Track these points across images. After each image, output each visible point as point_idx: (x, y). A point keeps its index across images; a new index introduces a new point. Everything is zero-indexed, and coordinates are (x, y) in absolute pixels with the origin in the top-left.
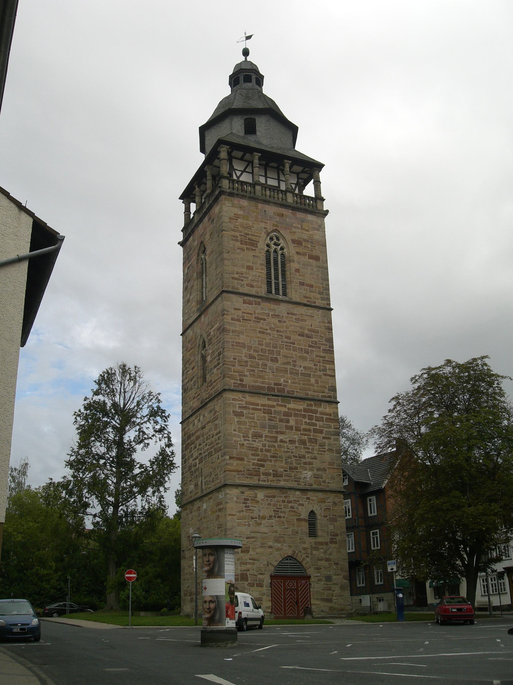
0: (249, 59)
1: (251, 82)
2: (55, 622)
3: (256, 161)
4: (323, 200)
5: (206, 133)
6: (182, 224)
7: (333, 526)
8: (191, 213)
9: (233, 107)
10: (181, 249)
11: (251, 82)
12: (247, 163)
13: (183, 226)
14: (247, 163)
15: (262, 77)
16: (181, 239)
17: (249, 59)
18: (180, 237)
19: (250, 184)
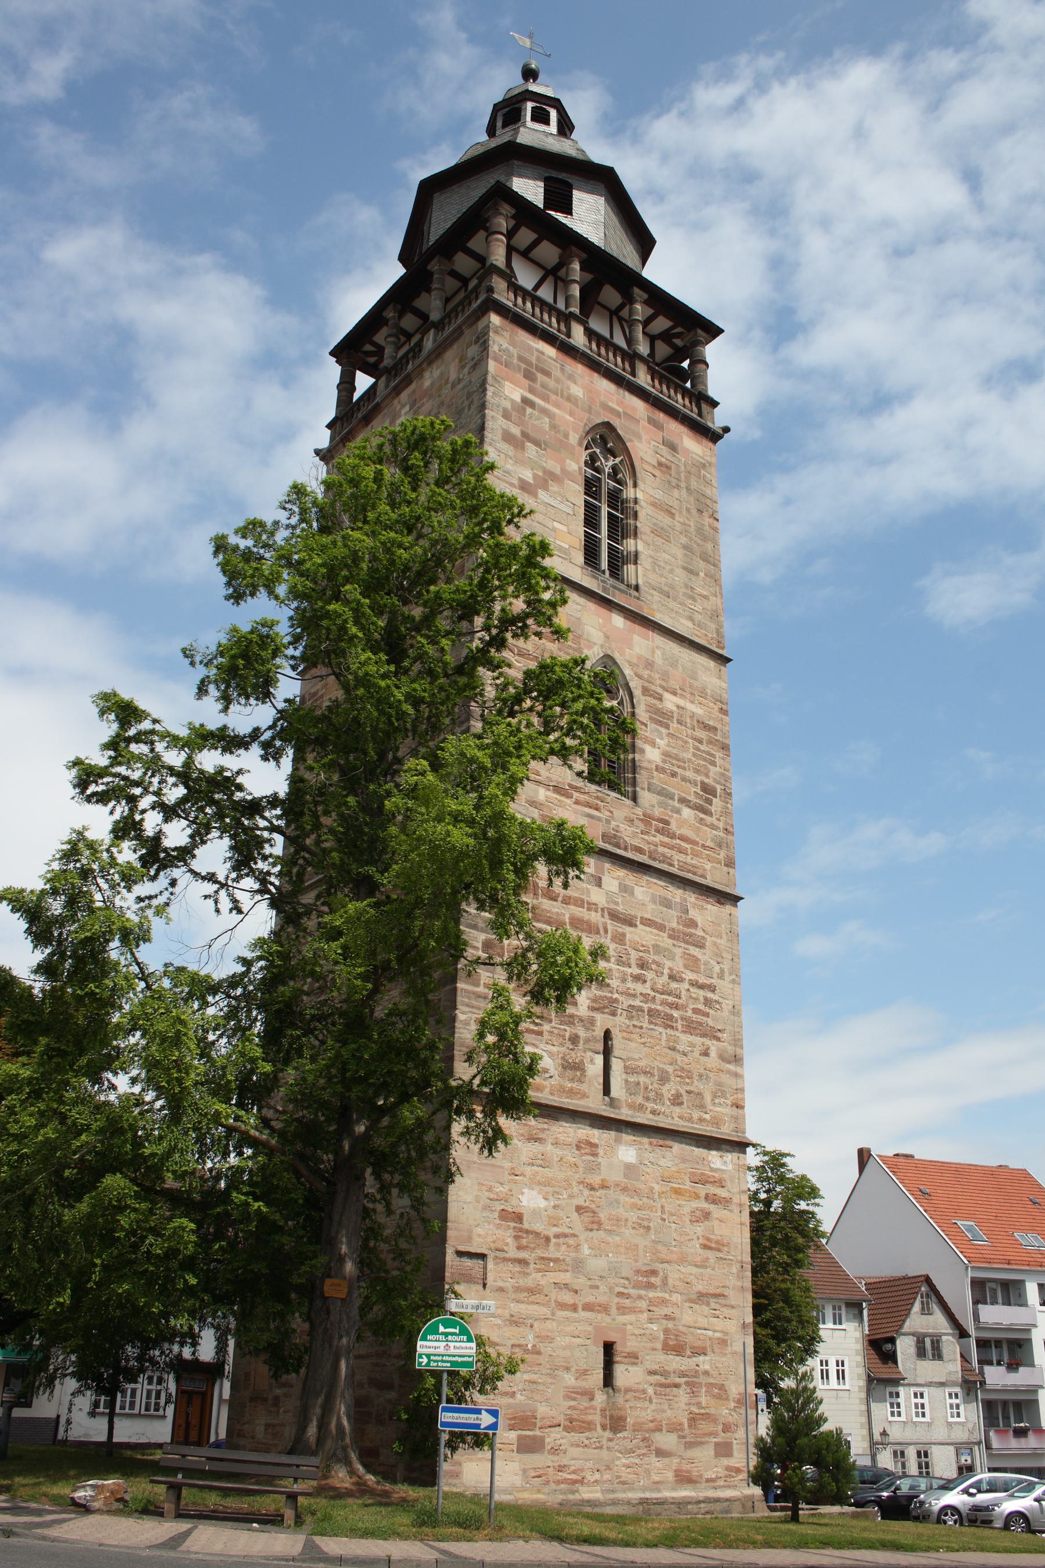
6: (330, 413)
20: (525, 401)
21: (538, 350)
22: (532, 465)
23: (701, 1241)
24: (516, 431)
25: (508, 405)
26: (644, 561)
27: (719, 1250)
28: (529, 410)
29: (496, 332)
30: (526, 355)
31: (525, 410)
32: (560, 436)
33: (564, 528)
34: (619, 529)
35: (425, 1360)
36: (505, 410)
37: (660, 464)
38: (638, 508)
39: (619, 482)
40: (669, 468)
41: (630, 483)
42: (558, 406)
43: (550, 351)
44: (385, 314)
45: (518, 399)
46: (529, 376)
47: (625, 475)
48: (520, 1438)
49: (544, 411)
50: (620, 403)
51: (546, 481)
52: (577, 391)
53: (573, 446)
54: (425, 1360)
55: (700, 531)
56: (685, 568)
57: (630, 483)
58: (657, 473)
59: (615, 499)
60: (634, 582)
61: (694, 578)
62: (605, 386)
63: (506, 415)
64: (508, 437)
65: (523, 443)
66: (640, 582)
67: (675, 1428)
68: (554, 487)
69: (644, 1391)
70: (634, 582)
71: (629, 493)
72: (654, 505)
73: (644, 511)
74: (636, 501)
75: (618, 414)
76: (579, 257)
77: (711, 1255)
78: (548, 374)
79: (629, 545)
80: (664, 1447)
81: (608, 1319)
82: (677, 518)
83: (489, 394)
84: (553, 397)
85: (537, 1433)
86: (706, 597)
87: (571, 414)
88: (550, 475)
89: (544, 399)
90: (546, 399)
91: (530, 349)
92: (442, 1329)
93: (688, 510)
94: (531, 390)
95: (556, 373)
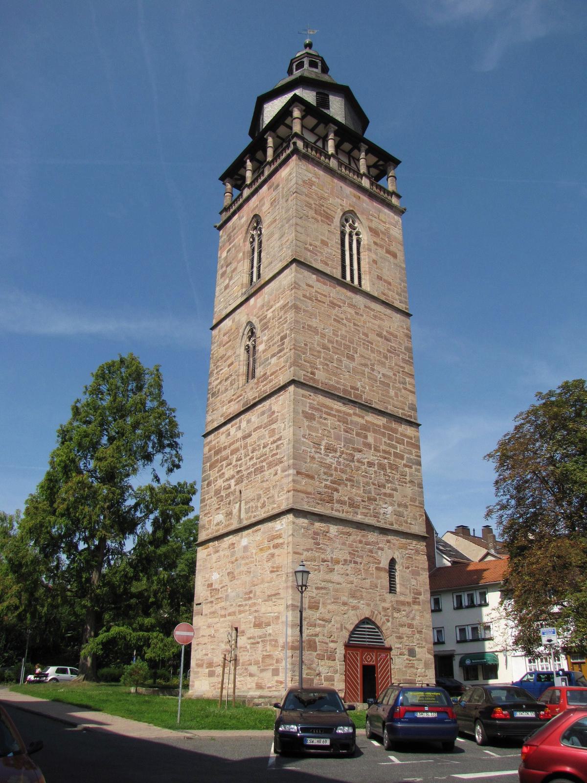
23: (271, 569)
27: (278, 571)
48: (209, 671)
67: (257, 663)
69: (246, 647)
77: (274, 575)
80: (252, 672)
81: (235, 617)
85: (214, 669)
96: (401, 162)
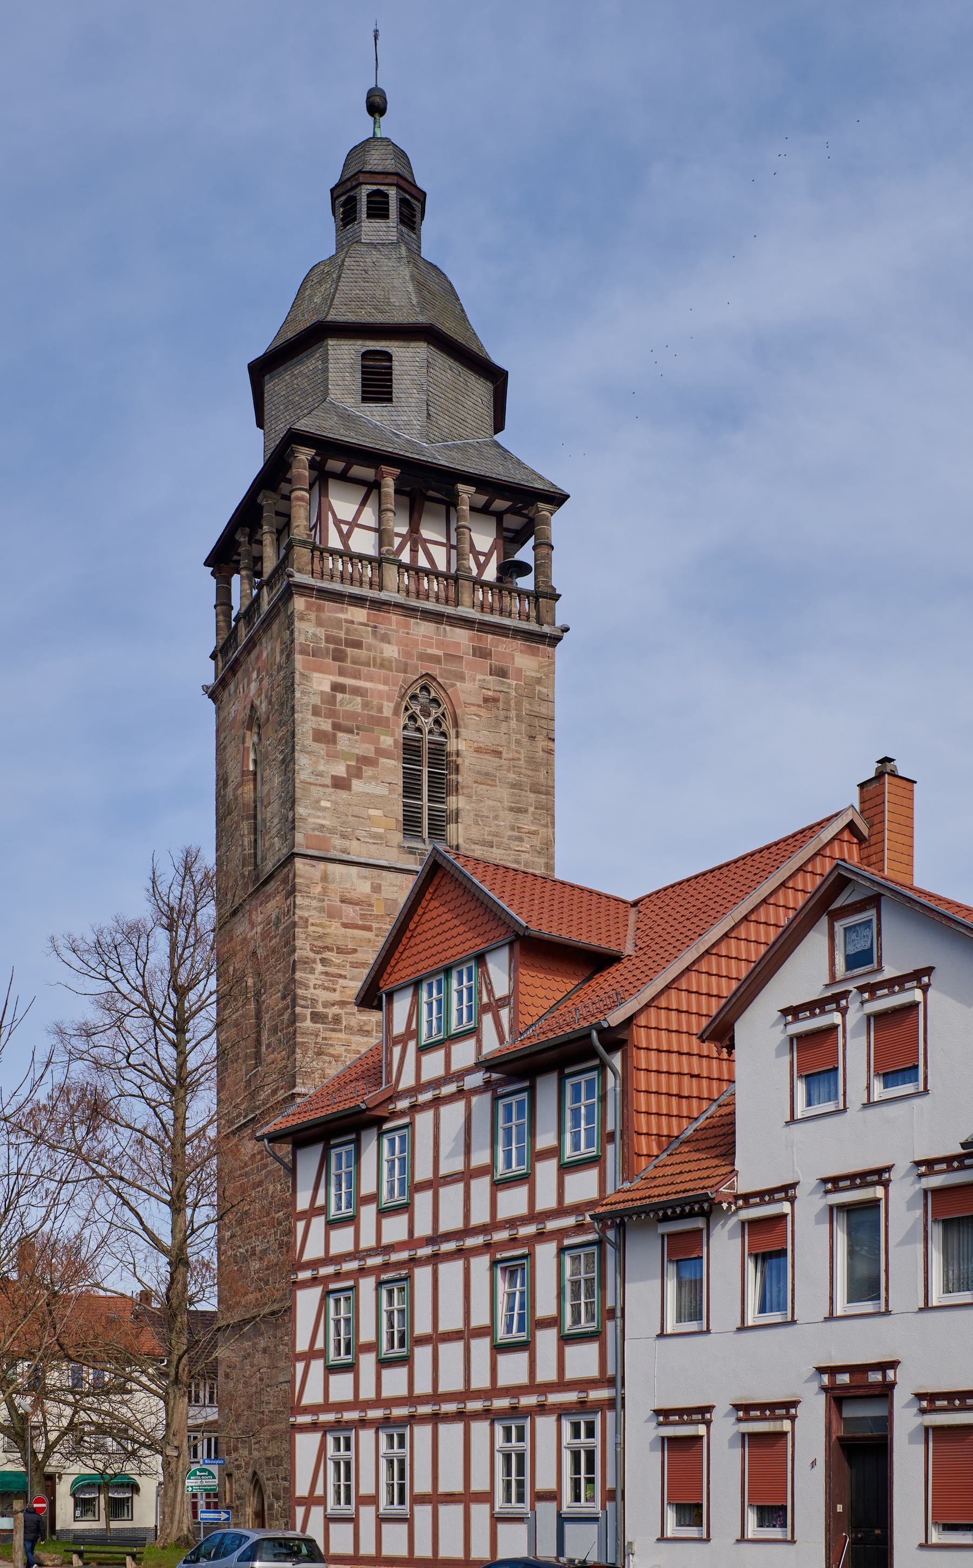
0: (388, 127)
1: (386, 216)
2: (831, 1299)
3: (389, 485)
4: (556, 597)
5: (268, 387)
6: (210, 642)
7: (159, 1458)
8: (232, 608)
9: (329, 318)
10: (211, 706)
11: (386, 216)
12: (363, 490)
13: (260, 464)
14: (363, 490)
15: (421, 196)
16: (210, 680)
17: (388, 127)
18: (208, 673)
19: (370, 560)
20: (337, 687)
21: (347, 621)
22: (345, 756)
24: (326, 725)
25: (316, 700)
26: (465, 819)
28: (339, 696)
29: (302, 619)
30: (334, 632)
31: (334, 697)
32: (374, 713)
33: (378, 813)
34: (441, 786)
35: (190, 1489)
36: (314, 707)
37: (486, 700)
38: (459, 761)
39: (443, 734)
40: (496, 700)
41: (452, 732)
42: (370, 679)
43: (359, 614)
44: (237, 537)
45: (327, 688)
46: (339, 656)
47: (447, 725)
49: (356, 691)
50: (441, 644)
51: (360, 769)
52: (391, 651)
53: (387, 718)
54: (190, 1489)
55: (531, 760)
56: (511, 809)
57: (452, 732)
58: (483, 712)
59: (439, 754)
60: (455, 843)
61: (520, 816)
62: (424, 629)
63: (316, 712)
64: (319, 736)
65: (334, 736)
66: (461, 841)
68: (368, 771)
70: (455, 843)
71: (452, 745)
72: (478, 750)
73: (468, 761)
74: (458, 754)
75: (436, 659)
76: (390, 474)
78: (358, 645)
79: (453, 802)
82: (504, 755)
83: (298, 694)
84: (364, 670)
86: (534, 833)
87: (386, 683)
88: (365, 760)
89: (355, 677)
90: (357, 676)
91: (338, 624)
92: (198, 1473)
93: (518, 742)
94: (342, 673)
95: (368, 639)
96: (568, 496)
